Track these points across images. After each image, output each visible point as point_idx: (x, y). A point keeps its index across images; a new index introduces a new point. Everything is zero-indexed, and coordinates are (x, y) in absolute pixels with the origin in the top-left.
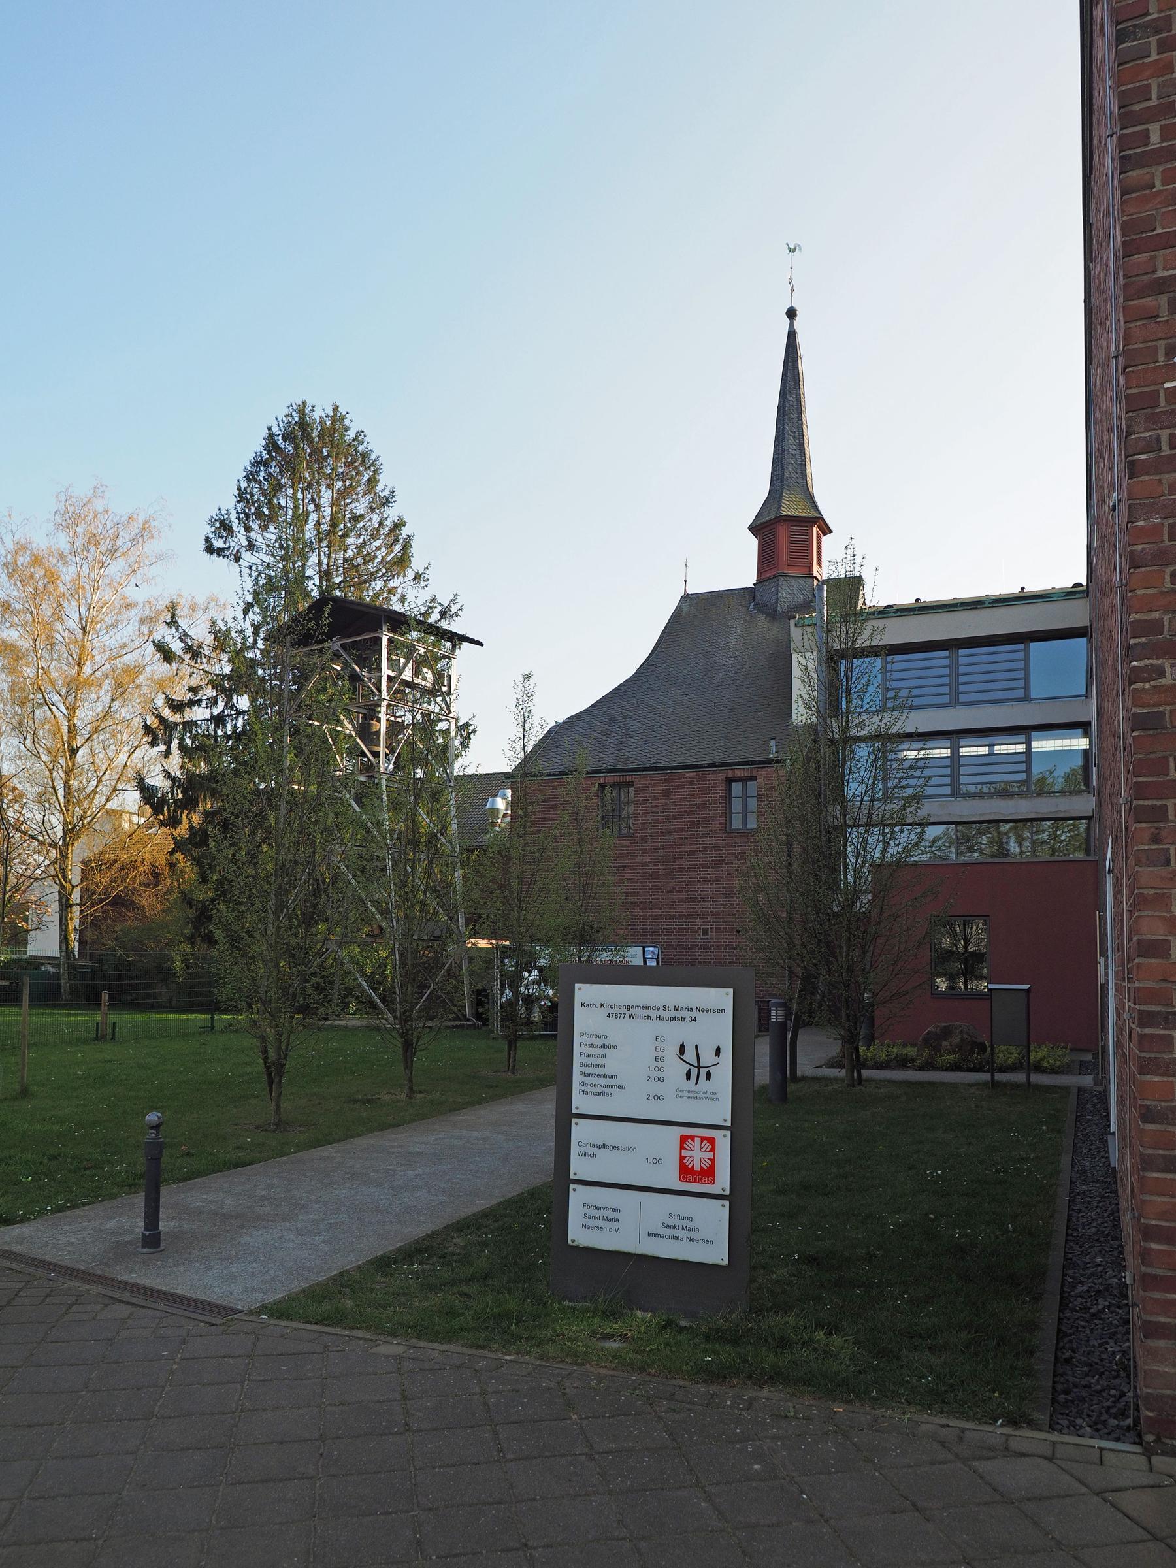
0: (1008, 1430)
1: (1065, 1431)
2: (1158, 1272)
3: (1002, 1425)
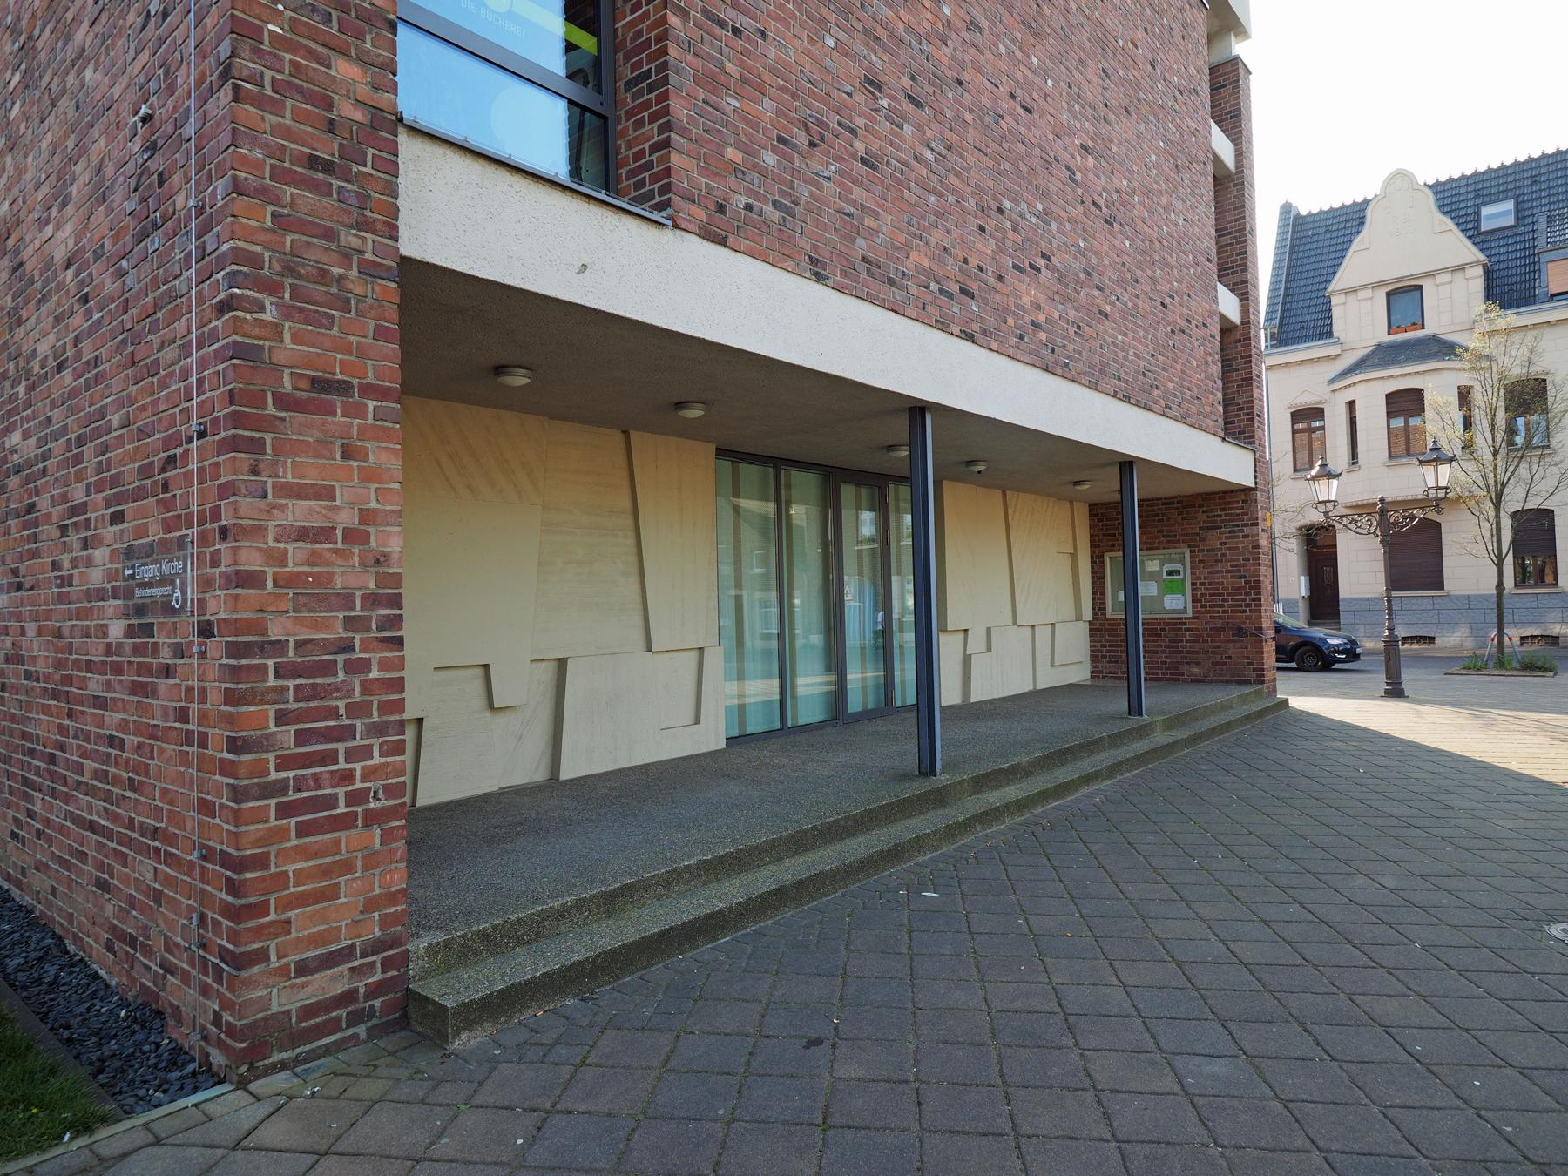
0: (82, 1141)
1: (139, 1109)
2: (251, 900)
3: (71, 1139)
